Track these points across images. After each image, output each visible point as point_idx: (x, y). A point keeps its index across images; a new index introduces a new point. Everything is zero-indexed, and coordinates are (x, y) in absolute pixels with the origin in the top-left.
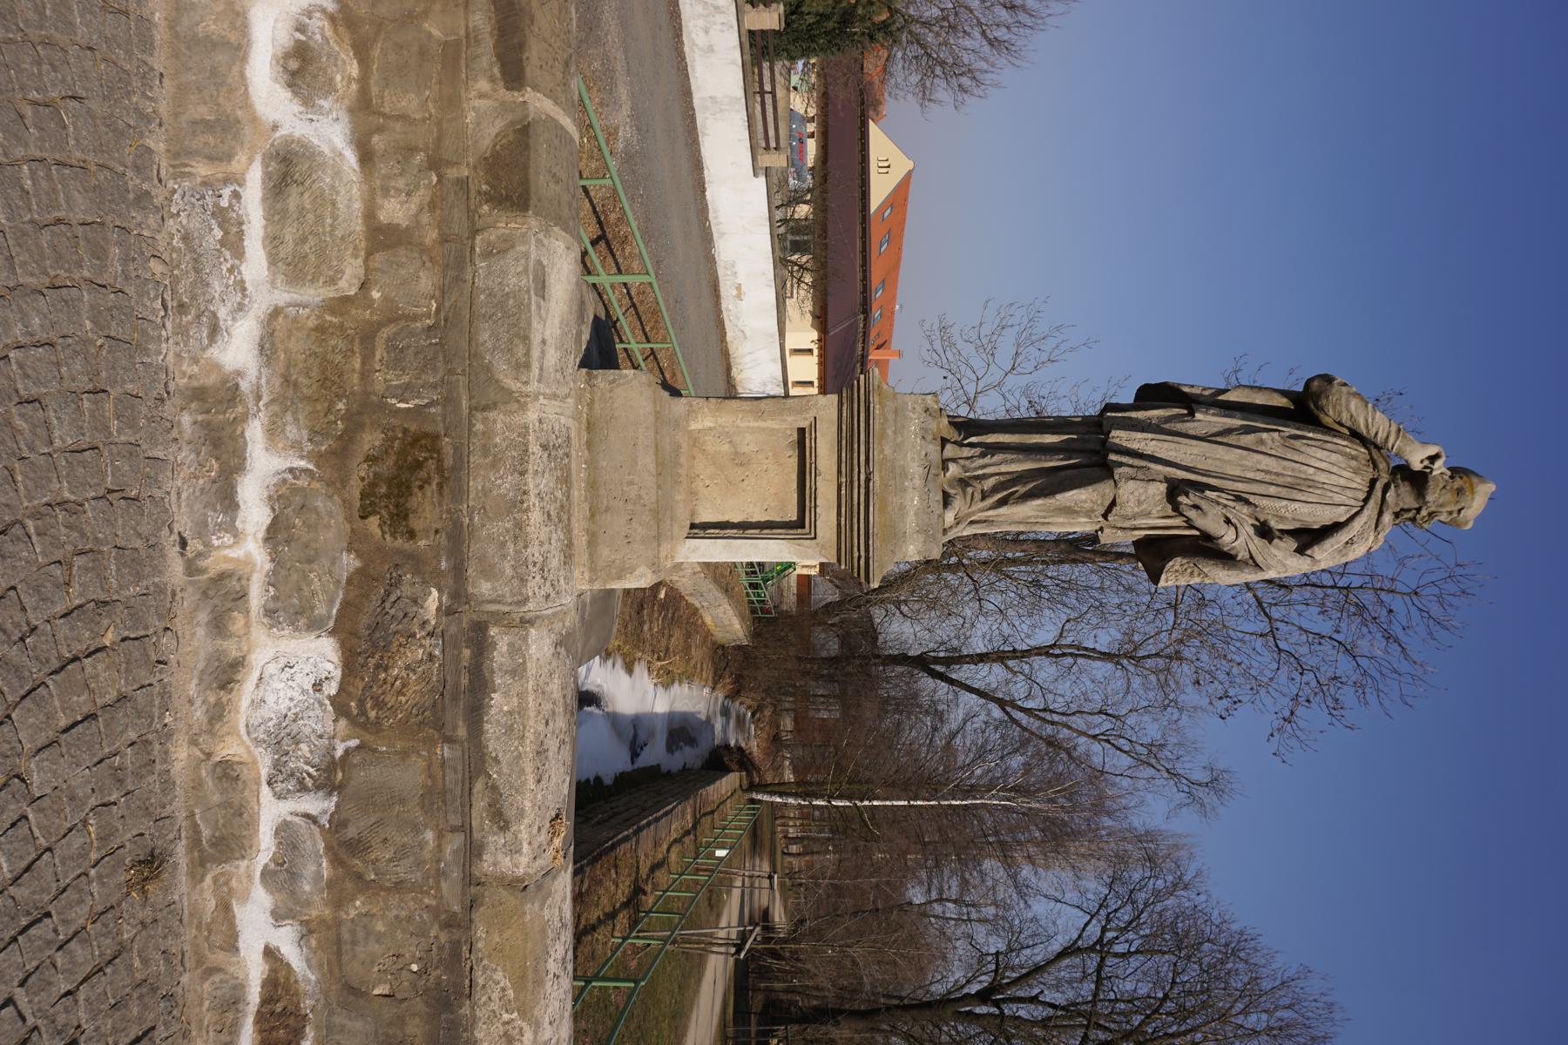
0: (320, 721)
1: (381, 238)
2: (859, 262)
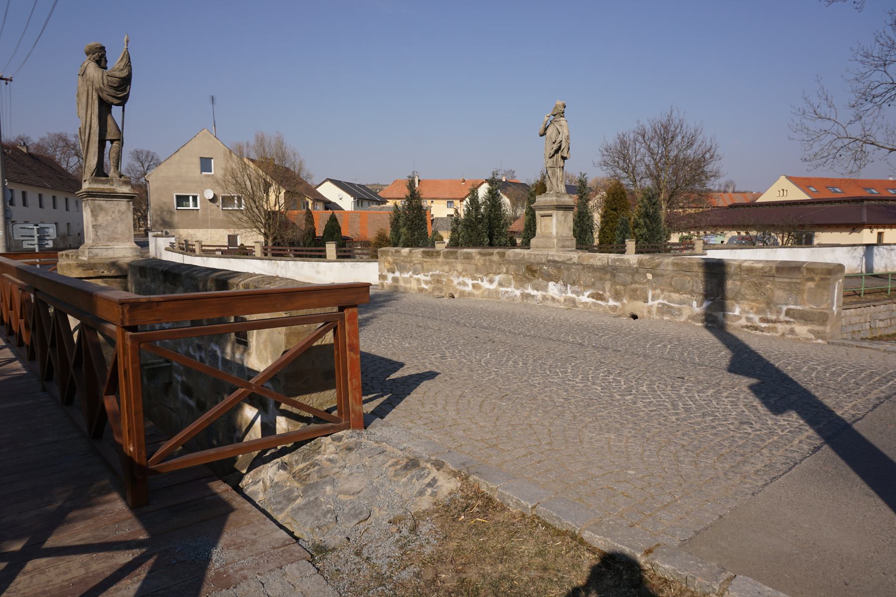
0: (559, 285)
1: (507, 272)
2: (828, 206)
